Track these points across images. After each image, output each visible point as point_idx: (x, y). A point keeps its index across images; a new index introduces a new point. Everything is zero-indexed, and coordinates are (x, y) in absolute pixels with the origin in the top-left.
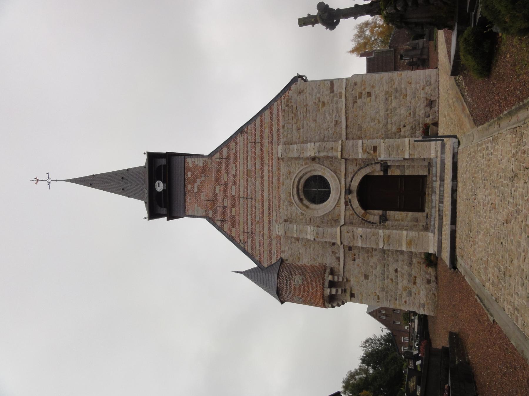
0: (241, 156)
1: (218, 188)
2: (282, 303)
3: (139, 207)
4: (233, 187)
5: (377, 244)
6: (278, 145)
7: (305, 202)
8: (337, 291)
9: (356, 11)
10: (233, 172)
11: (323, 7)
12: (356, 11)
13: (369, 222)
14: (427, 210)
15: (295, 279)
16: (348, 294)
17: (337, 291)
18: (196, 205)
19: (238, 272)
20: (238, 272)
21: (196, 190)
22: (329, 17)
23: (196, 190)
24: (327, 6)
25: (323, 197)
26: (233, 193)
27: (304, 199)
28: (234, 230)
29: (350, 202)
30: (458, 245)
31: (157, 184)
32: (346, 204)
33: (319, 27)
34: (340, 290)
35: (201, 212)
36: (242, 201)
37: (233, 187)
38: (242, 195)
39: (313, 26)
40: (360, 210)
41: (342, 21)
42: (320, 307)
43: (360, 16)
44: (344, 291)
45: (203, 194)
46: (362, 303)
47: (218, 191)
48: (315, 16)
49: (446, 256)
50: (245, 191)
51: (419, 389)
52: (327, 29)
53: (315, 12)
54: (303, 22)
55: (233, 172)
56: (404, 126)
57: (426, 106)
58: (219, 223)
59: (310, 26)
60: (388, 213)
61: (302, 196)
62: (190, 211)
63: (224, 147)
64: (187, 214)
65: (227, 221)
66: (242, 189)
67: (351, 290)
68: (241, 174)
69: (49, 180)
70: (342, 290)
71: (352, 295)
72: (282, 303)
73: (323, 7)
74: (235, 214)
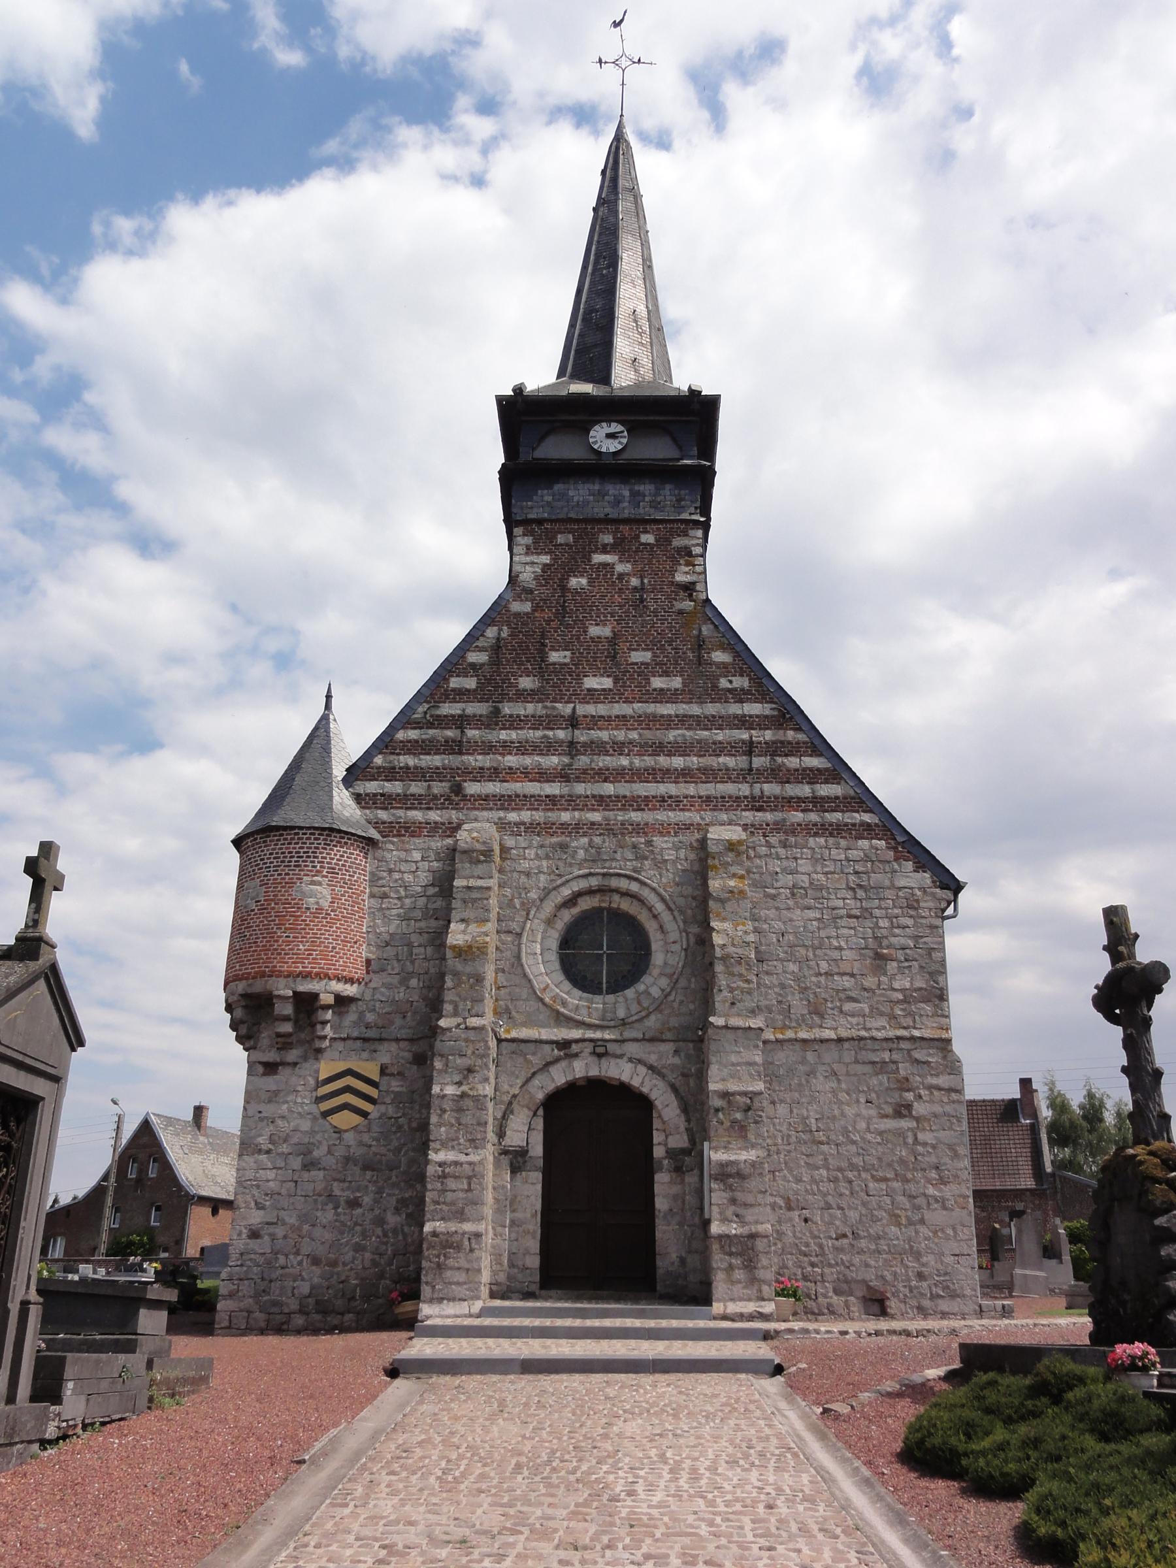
0: (711, 709)
1: (606, 631)
2: (237, 842)
3: (540, 370)
4: (607, 683)
5: (444, 1145)
6: (745, 827)
7: (567, 916)
8: (286, 1019)
9: (1143, 1074)
10: (657, 683)
11: (1152, 980)
12: (1143, 1074)
13: (289, 1064)
14: (544, 1292)
15: (320, 884)
16: (272, 1056)
17: (286, 1019)
18: (546, 559)
19: (329, 697)
20: (329, 697)
21: (598, 558)
22: (1126, 994)
23: (598, 558)
24: (1160, 991)
25: (576, 966)
26: (591, 682)
27: (575, 911)
28: (471, 683)
29: (567, 1056)
30: (472, 1382)
31: (615, 427)
32: (564, 1045)
33: (1103, 966)
34: (287, 1028)
35: (527, 576)
36: (567, 709)
37: (607, 683)
38: (581, 709)
39: (1105, 948)
40: (541, 1088)
41: (1118, 1032)
42: (229, 966)
43: (1131, 1085)
44: (284, 1043)
45: (584, 581)
46: (247, 1101)
47: (594, 631)
48: (1132, 955)
49: (421, 1348)
50: (595, 722)
51: (76, 1278)
52: (1097, 987)
53: (1144, 954)
54: (1115, 919)
55: (657, 683)
56: (806, 1220)
57: (869, 1288)
58: (491, 632)
59: (1105, 941)
60: (537, 1177)
61: (585, 904)
62: (528, 540)
63: (737, 655)
64: (518, 531)
65: (495, 661)
66: (602, 709)
67: (283, 1064)
68: (651, 708)
69: (624, 62)
70: (289, 1035)
71: (270, 1068)
72: (237, 842)
73: (1152, 980)
74: (521, 686)
